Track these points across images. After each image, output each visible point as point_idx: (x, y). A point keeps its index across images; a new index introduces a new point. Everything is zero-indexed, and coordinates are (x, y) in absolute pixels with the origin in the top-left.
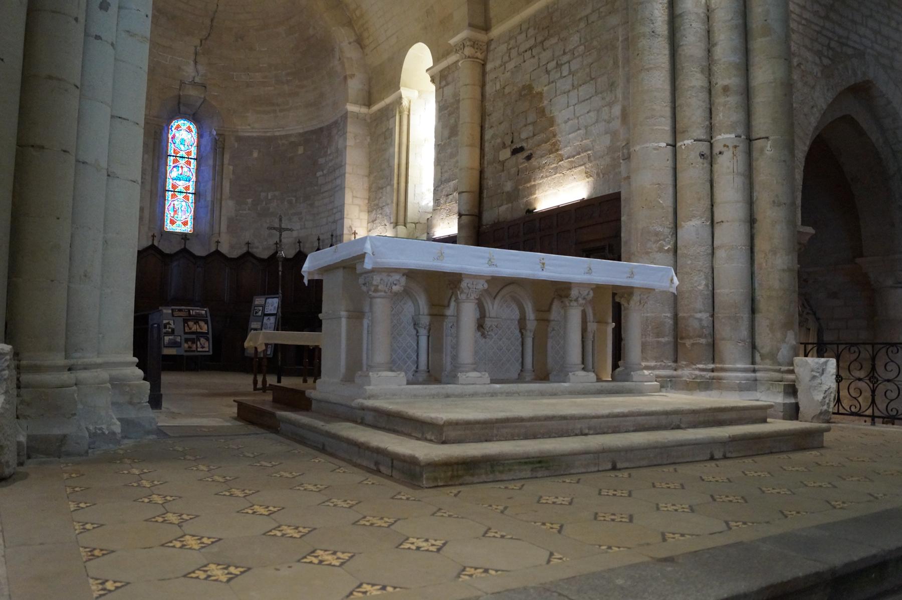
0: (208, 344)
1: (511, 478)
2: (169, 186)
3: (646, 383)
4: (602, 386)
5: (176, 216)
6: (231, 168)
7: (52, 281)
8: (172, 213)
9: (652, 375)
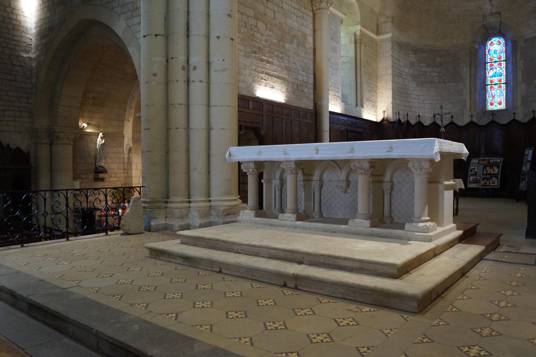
0: (497, 182)
1: (175, 262)
2: (489, 82)
3: (416, 233)
4: (372, 231)
5: (494, 100)
6: (522, 61)
7: (176, 173)
8: (491, 99)
9: (425, 227)
